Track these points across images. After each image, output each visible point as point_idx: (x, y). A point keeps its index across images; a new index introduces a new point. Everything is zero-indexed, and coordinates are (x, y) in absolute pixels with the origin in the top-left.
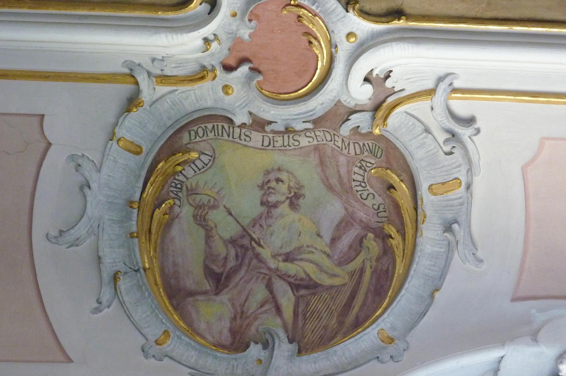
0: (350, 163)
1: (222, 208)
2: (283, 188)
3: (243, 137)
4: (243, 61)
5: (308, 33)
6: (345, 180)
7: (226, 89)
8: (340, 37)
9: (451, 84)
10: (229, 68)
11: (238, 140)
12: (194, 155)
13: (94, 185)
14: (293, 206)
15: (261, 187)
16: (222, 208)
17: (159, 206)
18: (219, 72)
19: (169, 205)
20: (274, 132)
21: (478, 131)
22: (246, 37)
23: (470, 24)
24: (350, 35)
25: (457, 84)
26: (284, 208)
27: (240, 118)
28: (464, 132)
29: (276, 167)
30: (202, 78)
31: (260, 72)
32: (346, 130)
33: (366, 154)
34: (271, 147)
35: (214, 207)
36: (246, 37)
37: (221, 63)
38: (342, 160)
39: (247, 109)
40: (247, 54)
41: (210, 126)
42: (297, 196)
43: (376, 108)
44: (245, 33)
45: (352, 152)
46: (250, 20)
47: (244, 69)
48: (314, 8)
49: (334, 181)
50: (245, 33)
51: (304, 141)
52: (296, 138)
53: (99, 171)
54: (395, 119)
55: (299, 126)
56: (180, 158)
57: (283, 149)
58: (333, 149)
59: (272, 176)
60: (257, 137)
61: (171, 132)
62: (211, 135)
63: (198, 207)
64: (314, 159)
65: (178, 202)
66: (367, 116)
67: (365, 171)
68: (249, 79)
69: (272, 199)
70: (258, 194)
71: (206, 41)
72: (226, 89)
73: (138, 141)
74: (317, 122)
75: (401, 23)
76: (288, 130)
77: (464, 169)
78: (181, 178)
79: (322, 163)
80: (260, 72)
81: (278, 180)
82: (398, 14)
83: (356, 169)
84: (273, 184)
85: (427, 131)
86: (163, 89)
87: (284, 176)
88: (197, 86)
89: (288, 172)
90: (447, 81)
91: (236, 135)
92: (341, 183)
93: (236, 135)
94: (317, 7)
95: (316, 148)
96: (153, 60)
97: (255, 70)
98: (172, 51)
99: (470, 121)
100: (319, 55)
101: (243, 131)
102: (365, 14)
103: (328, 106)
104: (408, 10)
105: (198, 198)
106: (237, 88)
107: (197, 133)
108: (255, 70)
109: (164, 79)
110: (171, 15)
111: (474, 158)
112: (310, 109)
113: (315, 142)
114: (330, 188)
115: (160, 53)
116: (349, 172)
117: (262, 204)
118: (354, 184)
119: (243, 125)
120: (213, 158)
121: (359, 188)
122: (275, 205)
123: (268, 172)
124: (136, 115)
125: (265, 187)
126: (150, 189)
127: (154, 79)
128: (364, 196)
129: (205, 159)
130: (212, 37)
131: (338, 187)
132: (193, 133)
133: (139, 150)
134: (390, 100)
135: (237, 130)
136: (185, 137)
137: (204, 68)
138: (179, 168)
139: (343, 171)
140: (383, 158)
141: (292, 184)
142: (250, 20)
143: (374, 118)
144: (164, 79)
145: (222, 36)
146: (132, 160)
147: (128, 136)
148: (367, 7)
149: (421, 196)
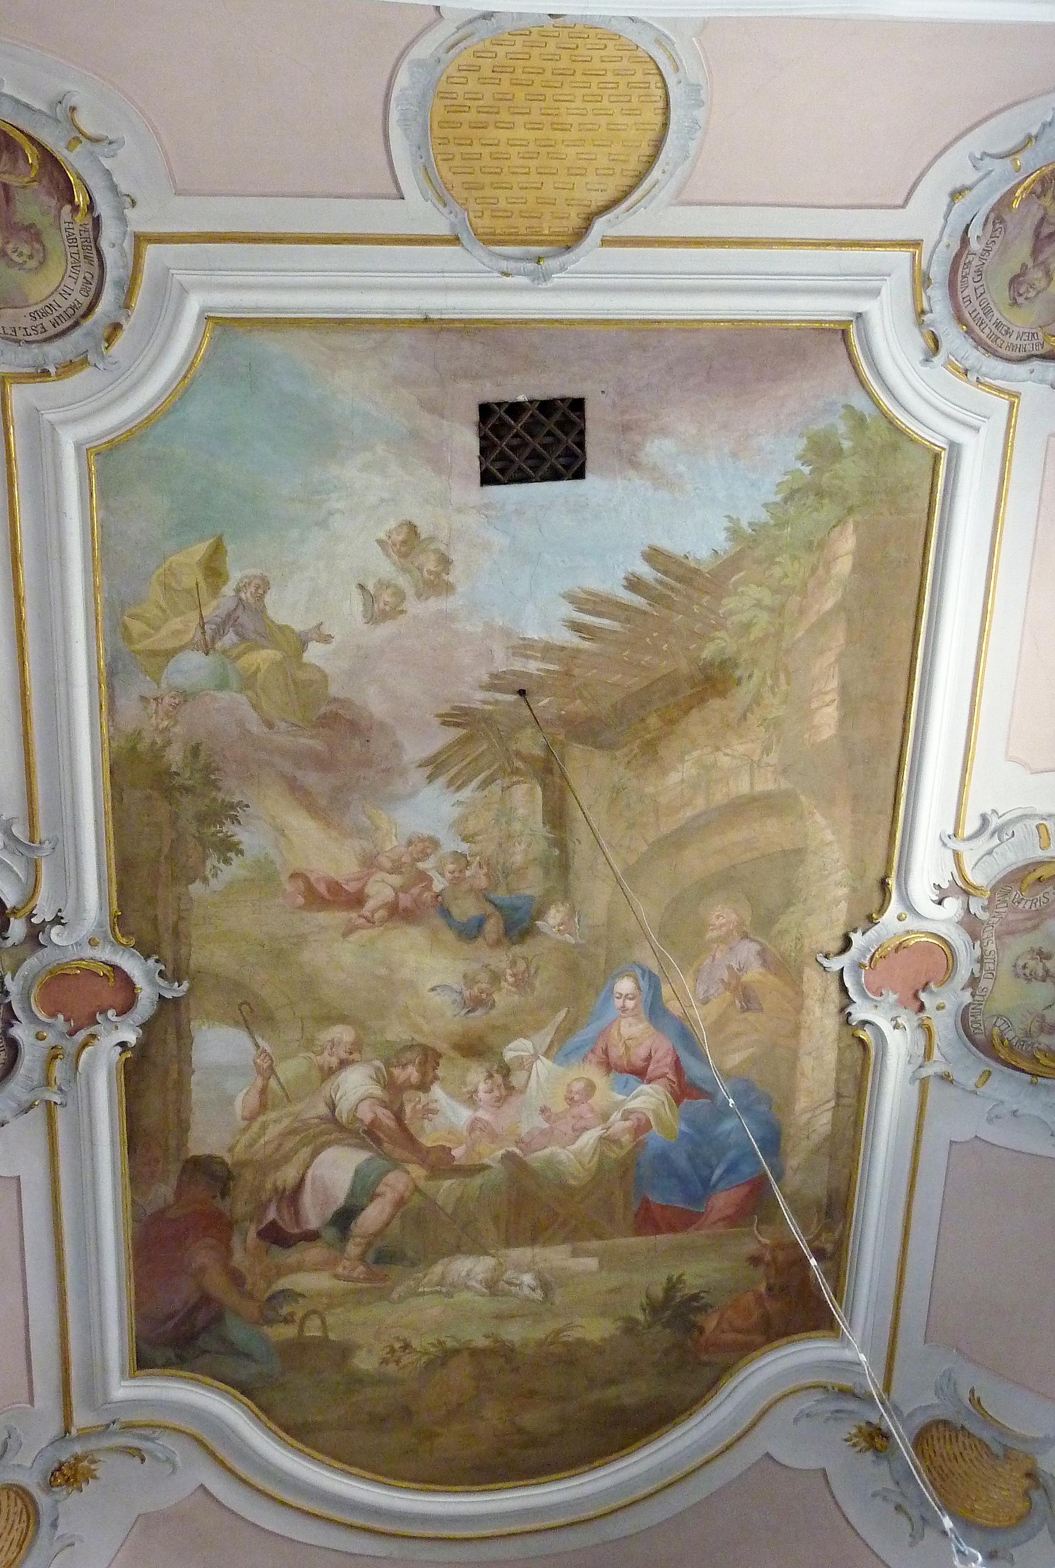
0: (1015, 911)
1: (1044, 1012)
2: (1031, 964)
3: (984, 994)
4: (916, 996)
5: (897, 950)
6: (1027, 915)
7: (940, 1008)
8: (900, 927)
9: (949, 837)
10: (922, 1008)
11: (985, 998)
12: (996, 1030)
13: (1015, 1107)
14: (1048, 957)
15: (1029, 980)
16: (1044, 1012)
17: (1038, 1060)
18: (923, 1015)
19: (1038, 1052)
20: (981, 969)
21: (994, 811)
22: (896, 997)
23: (897, 827)
24: (900, 918)
25: (951, 832)
26: (1049, 964)
27: (967, 998)
28: (994, 822)
29: (1013, 969)
30: (929, 1029)
31: (927, 984)
32: (983, 916)
33: (1007, 899)
34: (994, 973)
35: (1043, 1017)
36: (896, 997)
37: (916, 1013)
38: (1011, 917)
39: (959, 992)
40: (910, 993)
41: (971, 1019)
42: (1040, 953)
43: (967, 893)
44: (893, 997)
45: (1004, 910)
46: (881, 995)
47: (923, 996)
48: (873, 951)
49: (1029, 924)
50: (893, 997)
51: (992, 947)
52: (987, 953)
53: (1002, 1102)
54: (976, 878)
55: (978, 952)
56: (997, 1041)
57: (997, 963)
58: (1001, 925)
59: (1020, 971)
60: (983, 983)
61: (974, 1049)
62: (979, 1017)
63: (1042, 1030)
64: (1009, 940)
65: (1036, 1045)
66: (972, 900)
67: (1022, 899)
68: (932, 992)
69: (1040, 972)
70: (1034, 983)
71: (896, 1027)
72: (940, 1008)
73: (980, 1071)
74: (974, 936)
75: (892, 882)
76: (981, 960)
77: (1028, 822)
78: (1014, 1042)
79: (1012, 933)
80: (927, 984)
81: (1024, 967)
82: (883, 884)
83: (1020, 906)
84: (1027, 972)
85: (990, 853)
86: (936, 1054)
87: (1021, 963)
88: (934, 1029)
89: (1017, 960)
90: (946, 840)
91: (981, 998)
92: (1029, 919)
93: (981, 998)
94: (873, 947)
95: (998, 937)
96: (909, 1062)
97: (925, 987)
98: (903, 1051)
99: (985, 820)
100: (916, 940)
101: (978, 993)
102: (882, 910)
103: (961, 931)
104: (882, 874)
105: (1033, 1029)
106: (939, 1001)
107: (976, 1028)
108: (925, 987)
109: (928, 1054)
110: (873, 1053)
111: (1019, 813)
112: (962, 943)
113: (993, 939)
114: (1035, 927)
115: (904, 1058)
116: (1022, 912)
117: (1044, 981)
118: (1033, 908)
119: (973, 995)
120: (999, 1016)
121: (1038, 904)
122: (1047, 971)
123: (1017, 976)
124: (955, 1075)
125: (1029, 978)
126: (1023, 1065)
127: (926, 1063)
128: (1045, 900)
129: (1000, 1022)
130: (894, 1023)
131: (1036, 921)
132: (976, 1031)
133: (987, 1073)
134: (960, 883)
135: (977, 998)
136: (980, 1037)
137: (920, 1026)
138: (1006, 1042)
139: (1021, 916)
140: (1012, 885)
141: (1029, 957)
142: (881, 995)
143: (973, 895)
144: (928, 1054)
145: (894, 1014)
146: (994, 1081)
147: (974, 1080)
148: (876, 906)
149: (1047, 857)
